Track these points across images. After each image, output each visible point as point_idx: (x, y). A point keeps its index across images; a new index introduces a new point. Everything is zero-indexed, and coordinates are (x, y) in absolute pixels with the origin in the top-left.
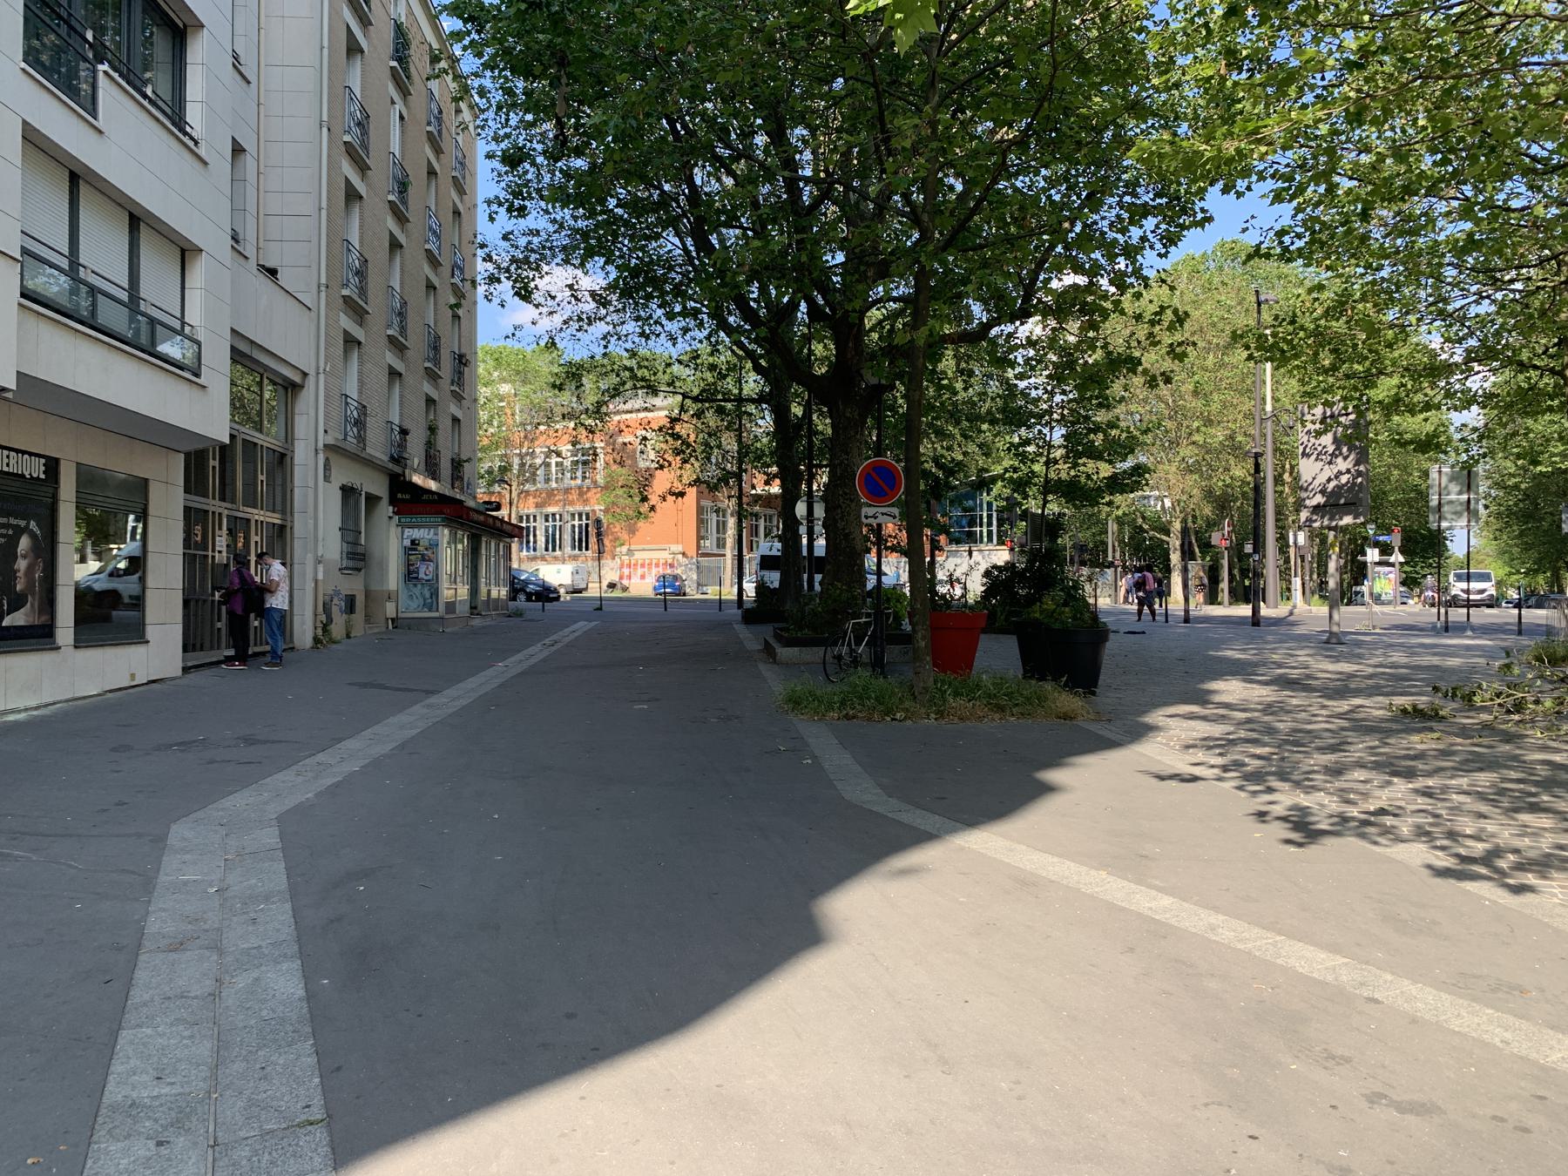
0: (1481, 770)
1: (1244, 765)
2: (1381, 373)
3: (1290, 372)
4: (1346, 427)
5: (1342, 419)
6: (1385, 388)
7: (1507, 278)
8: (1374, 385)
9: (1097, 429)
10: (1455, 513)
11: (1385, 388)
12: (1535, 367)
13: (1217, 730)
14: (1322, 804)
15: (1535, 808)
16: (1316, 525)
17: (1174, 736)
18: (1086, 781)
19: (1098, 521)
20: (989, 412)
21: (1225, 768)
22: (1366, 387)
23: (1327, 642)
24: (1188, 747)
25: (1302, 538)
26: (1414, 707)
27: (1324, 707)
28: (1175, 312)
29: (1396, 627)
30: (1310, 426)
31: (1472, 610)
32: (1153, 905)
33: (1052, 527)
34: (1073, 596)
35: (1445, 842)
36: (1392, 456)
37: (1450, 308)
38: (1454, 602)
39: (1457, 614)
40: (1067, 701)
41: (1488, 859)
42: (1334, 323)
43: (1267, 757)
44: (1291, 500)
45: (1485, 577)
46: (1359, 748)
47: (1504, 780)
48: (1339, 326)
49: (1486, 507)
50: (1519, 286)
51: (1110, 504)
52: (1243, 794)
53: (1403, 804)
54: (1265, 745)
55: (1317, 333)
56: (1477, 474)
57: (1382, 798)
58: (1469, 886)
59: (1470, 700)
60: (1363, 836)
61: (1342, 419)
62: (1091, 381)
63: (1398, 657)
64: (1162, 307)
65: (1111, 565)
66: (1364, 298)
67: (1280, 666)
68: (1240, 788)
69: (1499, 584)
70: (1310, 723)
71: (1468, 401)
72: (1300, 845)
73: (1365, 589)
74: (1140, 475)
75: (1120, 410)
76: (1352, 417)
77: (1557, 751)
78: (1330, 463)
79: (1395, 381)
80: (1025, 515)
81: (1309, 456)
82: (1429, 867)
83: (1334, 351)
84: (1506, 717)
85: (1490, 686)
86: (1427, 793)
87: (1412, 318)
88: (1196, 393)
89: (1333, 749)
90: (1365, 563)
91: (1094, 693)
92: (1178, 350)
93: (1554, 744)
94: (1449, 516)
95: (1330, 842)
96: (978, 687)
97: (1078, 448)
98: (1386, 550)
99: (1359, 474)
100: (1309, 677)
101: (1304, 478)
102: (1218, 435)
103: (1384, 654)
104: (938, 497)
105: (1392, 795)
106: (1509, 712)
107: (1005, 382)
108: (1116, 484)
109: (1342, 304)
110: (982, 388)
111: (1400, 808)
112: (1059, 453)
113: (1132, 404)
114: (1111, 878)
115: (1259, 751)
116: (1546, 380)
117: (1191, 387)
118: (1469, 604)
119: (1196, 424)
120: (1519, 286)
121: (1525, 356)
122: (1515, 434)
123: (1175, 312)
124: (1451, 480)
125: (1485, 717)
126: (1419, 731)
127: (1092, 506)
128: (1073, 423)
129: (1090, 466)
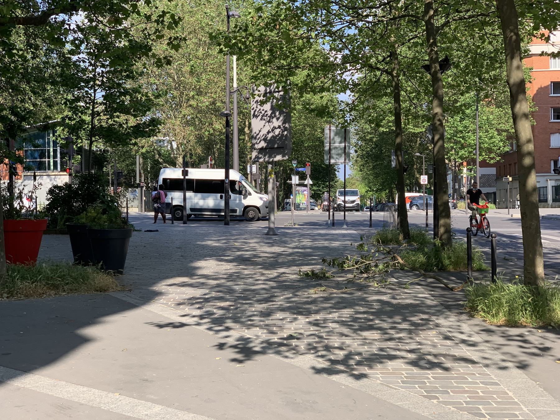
0: (345, 307)
1: (214, 314)
2: (297, 67)
3: (245, 62)
4: (278, 100)
5: (276, 95)
6: (300, 76)
7: (365, 14)
8: (292, 74)
9: (126, 93)
10: (338, 154)
11: (300, 76)
12: (378, 69)
13: (198, 293)
14: (256, 335)
15: (371, 328)
16: (261, 160)
17: (172, 299)
18: (115, 334)
19: (131, 156)
20: (51, 76)
21: (201, 317)
22: (289, 75)
23: (267, 234)
24: (179, 304)
25: (254, 169)
26: (313, 271)
27: (263, 274)
28: (173, 16)
29: (306, 224)
30: (257, 98)
31: (346, 213)
32: (148, 412)
33: (99, 160)
34: (111, 207)
35: (324, 353)
36: (306, 118)
37: (334, 29)
38: (339, 208)
39: (339, 215)
40: (102, 279)
41: (345, 361)
42: (269, 33)
43: (226, 308)
44: (249, 145)
45: (354, 193)
46: (280, 300)
47: (358, 313)
48: (272, 35)
49: (356, 151)
50: (370, 19)
51: (135, 144)
52: (211, 333)
53: (302, 331)
54: (227, 300)
55: (260, 38)
56: (349, 131)
57: (290, 329)
58: (334, 378)
59: (342, 267)
60: (278, 353)
61: (276, 95)
62: (123, 58)
63: (307, 242)
64: (163, 12)
65: (138, 186)
66: (285, 19)
67: (239, 250)
68: (210, 329)
69: (362, 198)
70: (254, 285)
71: (344, 87)
72: (240, 362)
73: (290, 201)
74: (154, 126)
75: (142, 81)
76: (282, 93)
77: (385, 294)
78: (269, 122)
79: (305, 72)
80: (80, 150)
81: (257, 117)
82: (313, 368)
83: (270, 51)
84: (360, 276)
85: (353, 257)
86: (316, 324)
87: (313, 34)
88: (192, 73)
89: (266, 300)
90: (291, 185)
91: (121, 273)
92: (175, 43)
93: (383, 290)
94: (335, 156)
95: (259, 358)
96: (40, 272)
97: (113, 105)
98: (303, 177)
99: (285, 129)
100: (255, 256)
101: (254, 132)
102: (205, 101)
103: (299, 241)
104: (14, 136)
105: (297, 326)
106: (362, 273)
107: (61, 55)
108: (140, 131)
109: (274, 21)
110: (44, 58)
111: (301, 334)
112: (100, 108)
113: (149, 79)
114: (123, 397)
115: (223, 304)
116: (383, 77)
117: (188, 69)
118: (345, 209)
119: (192, 93)
120: (370, 19)
121: (373, 61)
122: (368, 108)
123: (173, 16)
124: (335, 135)
125: (350, 276)
126: (314, 286)
127: (123, 145)
128: (110, 88)
129: (123, 118)
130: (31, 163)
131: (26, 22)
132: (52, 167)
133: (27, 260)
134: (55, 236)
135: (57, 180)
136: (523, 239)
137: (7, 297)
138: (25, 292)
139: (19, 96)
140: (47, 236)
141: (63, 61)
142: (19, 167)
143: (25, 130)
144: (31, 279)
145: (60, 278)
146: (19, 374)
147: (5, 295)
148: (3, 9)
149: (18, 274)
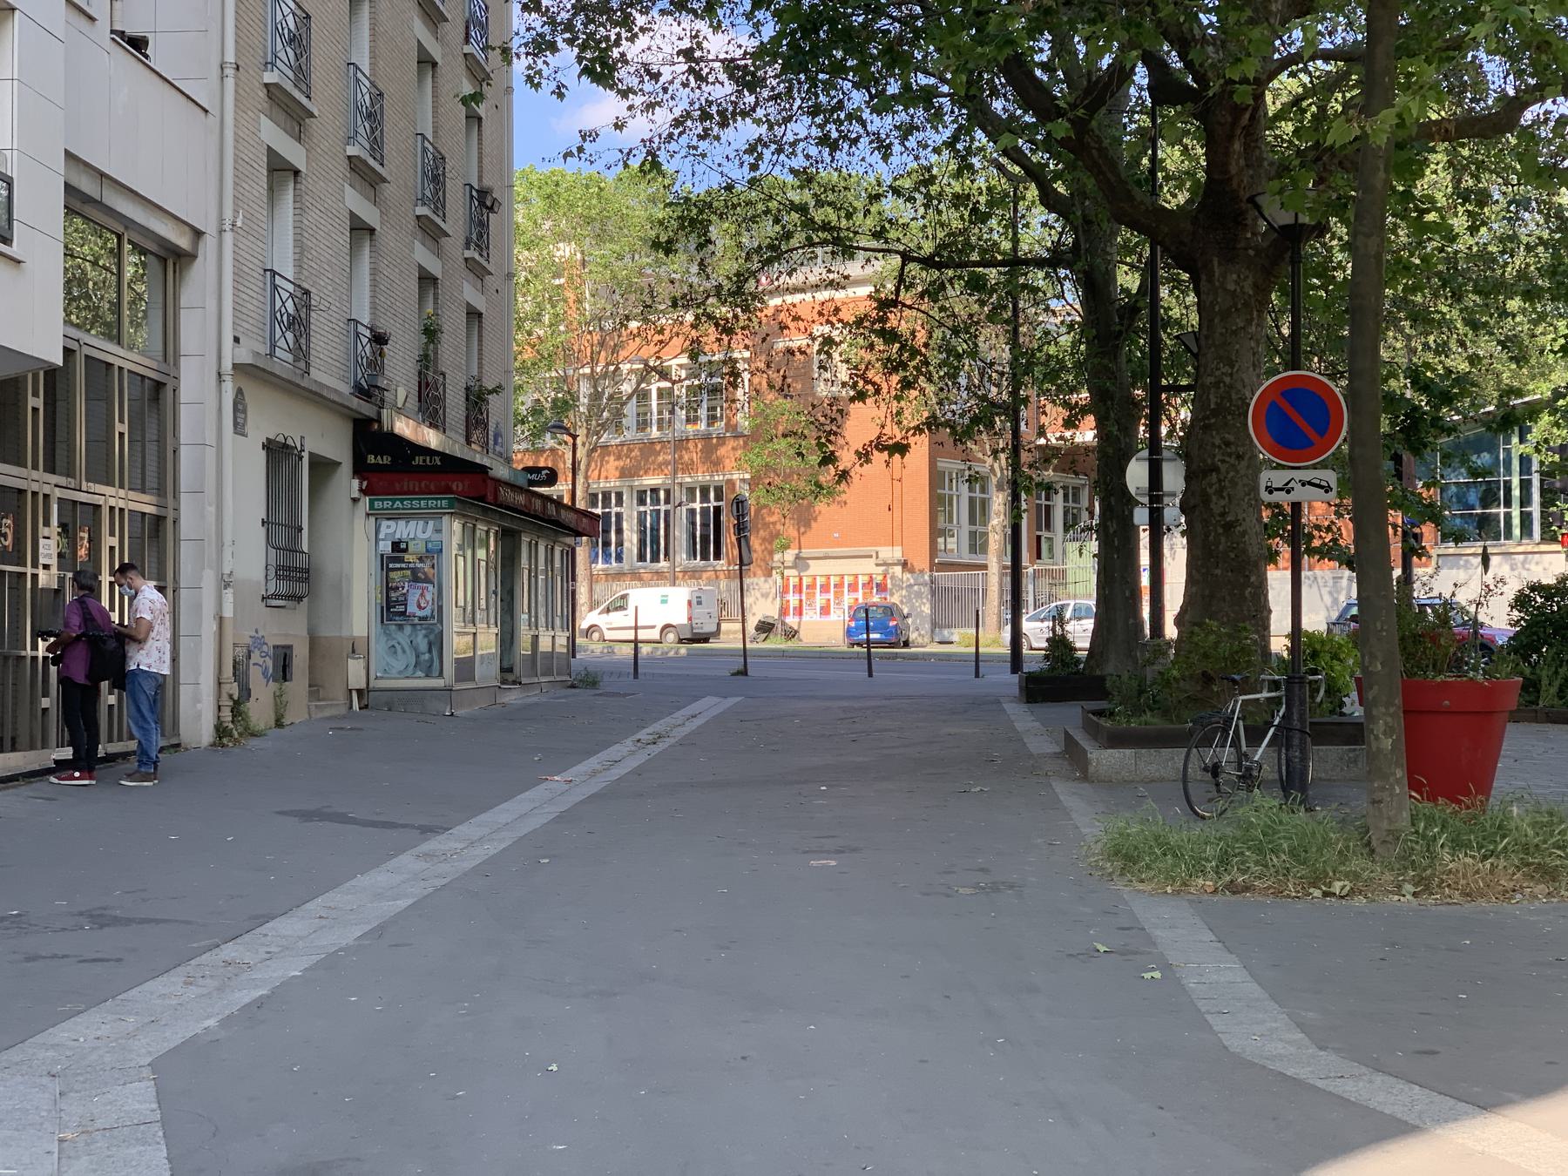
20: (1522, 274)
104: (1418, 448)
130: (1458, 521)
131: (1453, 132)
132: (1517, 532)
133: (1467, 793)
134: (1535, 727)
135: (1533, 567)
136: (1359, 605)
137: (1415, 894)
138: (1462, 882)
139: (1431, 338)
140: (1521, 726)
141: (1558, 229)
142: (1428, 531)
143: (1451, 429)
144: (1480, 847)
145: (1559, 848)
146: (1466, 1113)
147: (1409, 888)
148: (1411, 104)
149: (1442, 831)
